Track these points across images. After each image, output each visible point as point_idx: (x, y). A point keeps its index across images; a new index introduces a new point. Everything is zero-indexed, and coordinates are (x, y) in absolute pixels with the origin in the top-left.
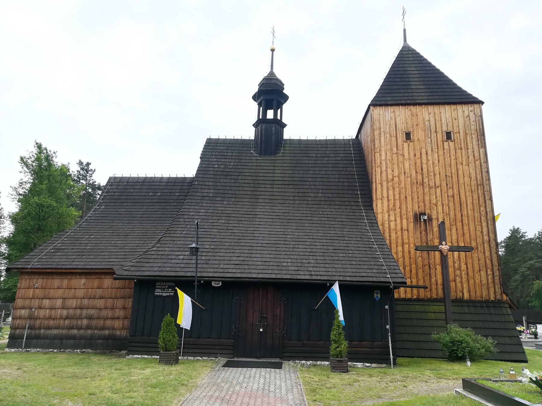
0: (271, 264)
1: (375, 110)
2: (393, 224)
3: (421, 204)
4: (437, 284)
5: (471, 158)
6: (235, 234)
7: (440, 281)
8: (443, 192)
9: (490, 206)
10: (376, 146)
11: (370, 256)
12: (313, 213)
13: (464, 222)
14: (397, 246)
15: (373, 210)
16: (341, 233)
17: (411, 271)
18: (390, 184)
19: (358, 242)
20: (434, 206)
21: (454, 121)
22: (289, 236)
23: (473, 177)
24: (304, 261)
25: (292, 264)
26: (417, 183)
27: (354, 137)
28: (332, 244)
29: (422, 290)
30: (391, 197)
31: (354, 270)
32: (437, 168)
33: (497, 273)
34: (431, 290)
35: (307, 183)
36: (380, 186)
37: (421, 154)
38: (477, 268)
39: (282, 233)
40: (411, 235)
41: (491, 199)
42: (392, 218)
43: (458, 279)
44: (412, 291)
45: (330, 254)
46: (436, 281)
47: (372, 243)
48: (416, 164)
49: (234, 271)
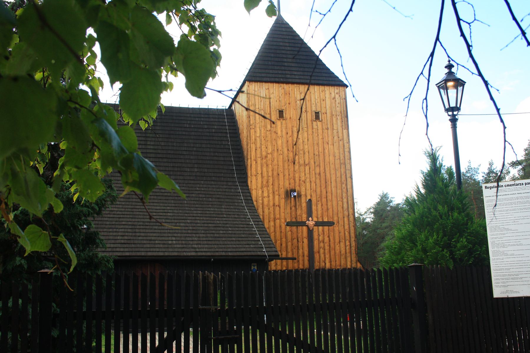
0: (157, 242)
1: (250, 86)
2: (266, 200)
3: (292, 181)
4: (303, 256)
5: (336, 138)
6: (113, 212)
7: (306, 253)
8: (311, 170)
9: (350, 183)
10: (251, 122)
11: (248, 232)
12: (190, 189)
13: (328, 198)
14: (269, 222)
15: (248, 186)
16: (219, 210)
17: (281, 245)
18: (264, 161)
19: (235, 219)
20: (303, 183)
21: (322, 102)
22: (169, 214)
23: (337, 157)
24: (188, 239)
25: (177, 242)
26: (289, 160)
27: (227, 108)
28: (212, 222)
29: (290, 261)
30: (265, 174)
31: (234, 246)
32: (306, 147)
33: (353, 244)
34: (298, 261)
35: (182, 157)
36: (255, 162)
37: (292, 132)
38: (337, 240)
39: (161, 211)
40: (282, 210)
41: (351, 178)
42: (266, 194)
43: (322, 251)
44: (282, 263)
45: (211, 232)
46: (303, 253)
47: (248, 220)
48: (287, 141)
49: (122, 250)
